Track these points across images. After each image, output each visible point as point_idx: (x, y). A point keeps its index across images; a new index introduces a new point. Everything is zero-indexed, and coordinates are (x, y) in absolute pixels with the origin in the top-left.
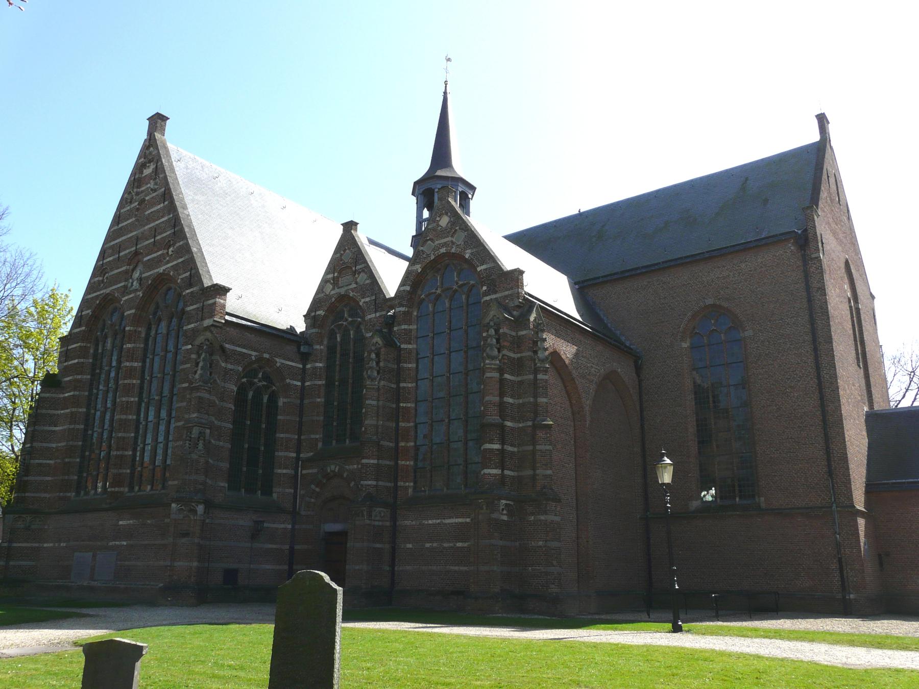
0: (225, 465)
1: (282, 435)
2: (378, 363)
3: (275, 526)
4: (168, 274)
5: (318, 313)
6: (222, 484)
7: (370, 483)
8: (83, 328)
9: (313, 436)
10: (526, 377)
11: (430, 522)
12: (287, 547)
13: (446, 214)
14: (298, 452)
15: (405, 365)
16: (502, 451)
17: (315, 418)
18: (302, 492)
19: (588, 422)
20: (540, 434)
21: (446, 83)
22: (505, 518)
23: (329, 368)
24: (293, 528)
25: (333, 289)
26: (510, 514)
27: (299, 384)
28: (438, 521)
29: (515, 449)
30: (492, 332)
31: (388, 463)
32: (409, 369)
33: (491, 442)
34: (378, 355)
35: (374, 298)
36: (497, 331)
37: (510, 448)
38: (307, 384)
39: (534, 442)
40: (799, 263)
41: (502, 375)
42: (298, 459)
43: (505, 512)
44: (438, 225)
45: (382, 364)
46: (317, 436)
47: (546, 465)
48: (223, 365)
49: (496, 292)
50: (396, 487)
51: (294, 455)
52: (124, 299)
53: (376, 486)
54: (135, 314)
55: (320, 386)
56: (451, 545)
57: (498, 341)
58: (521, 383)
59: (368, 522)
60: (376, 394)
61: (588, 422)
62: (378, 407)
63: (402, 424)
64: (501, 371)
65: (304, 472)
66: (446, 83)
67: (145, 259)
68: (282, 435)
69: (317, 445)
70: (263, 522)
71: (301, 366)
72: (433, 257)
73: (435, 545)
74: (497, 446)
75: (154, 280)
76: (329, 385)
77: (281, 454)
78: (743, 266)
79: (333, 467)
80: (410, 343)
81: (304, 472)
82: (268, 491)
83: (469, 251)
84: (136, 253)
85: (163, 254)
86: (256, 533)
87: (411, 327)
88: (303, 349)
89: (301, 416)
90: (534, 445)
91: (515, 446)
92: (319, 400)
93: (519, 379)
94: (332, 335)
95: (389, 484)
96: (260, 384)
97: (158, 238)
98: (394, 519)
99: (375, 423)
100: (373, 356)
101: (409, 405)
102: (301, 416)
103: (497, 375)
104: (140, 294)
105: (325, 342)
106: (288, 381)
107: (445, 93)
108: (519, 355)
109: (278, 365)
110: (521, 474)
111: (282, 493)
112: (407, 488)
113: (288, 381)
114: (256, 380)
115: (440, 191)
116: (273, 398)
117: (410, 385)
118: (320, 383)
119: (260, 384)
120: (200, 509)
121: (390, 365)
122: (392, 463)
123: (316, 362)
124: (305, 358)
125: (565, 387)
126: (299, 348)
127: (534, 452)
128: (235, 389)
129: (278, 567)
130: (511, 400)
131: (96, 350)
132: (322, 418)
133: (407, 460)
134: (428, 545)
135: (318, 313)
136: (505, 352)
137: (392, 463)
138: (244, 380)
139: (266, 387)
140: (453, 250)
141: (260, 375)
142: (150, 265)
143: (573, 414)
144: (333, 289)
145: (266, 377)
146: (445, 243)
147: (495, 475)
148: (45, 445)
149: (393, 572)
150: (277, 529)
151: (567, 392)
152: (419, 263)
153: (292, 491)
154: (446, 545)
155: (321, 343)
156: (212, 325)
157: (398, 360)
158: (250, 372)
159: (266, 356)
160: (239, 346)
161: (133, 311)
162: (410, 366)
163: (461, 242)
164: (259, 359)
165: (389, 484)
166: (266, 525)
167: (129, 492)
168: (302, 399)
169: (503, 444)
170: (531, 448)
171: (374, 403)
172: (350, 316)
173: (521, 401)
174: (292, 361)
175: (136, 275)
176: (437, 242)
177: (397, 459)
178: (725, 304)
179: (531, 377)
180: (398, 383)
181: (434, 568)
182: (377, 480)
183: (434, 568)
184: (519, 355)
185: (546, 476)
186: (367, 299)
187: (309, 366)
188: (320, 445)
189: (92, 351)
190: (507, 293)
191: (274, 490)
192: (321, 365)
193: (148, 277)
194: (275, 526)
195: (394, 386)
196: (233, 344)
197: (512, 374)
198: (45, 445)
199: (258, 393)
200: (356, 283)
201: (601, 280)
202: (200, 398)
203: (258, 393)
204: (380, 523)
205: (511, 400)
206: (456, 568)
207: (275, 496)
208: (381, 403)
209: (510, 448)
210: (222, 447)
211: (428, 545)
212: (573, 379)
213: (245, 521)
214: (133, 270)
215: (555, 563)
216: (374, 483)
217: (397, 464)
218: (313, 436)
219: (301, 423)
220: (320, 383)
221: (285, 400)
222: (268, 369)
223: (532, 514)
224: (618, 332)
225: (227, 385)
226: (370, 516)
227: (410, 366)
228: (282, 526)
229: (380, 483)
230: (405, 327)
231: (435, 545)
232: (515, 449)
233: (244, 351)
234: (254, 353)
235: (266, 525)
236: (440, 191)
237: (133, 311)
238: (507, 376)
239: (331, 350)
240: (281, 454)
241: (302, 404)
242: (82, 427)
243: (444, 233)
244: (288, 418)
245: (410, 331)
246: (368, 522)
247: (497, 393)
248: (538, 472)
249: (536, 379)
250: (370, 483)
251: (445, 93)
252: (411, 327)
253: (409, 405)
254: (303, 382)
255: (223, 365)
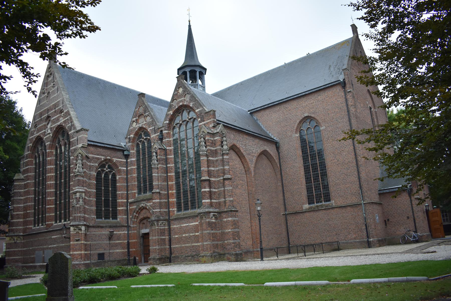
0: (94, 208)
1: (119, 192)
2: (157, 157)
3: (120, 232)
4: (62, 125)
5: (131, 136)
6: (93, 217)
7: (157, 210)
8: (29, 152)
9: (133, 192)
10: (218, 158)
11: (184, 225)
12: (126, 241)
13: (181, 87)
14: (127, 199)
15: (169, 157)
16: (210, 192)
17: (133, 183)
18: (131, 217)
19: (253, 174)
20: (227, 182)
21: (189, 22)
22: (214, 221)
23: (138, 160)
24: (128, 233)
25: (136, 125)
26: (216, 218)
27: (125, 169)
28: (188, 224)
29: (217, 190)
30: (202, 139)
31: (165, 201)
32: (171, 158)
33: (205, 188)
34: (156, 153)
35: (153, 127)
36: (204, 139)
37: (214, 190)
38: (129, 168)
39: (224, 186)
40: (343, 94)
41: (208, 158)
42: (127, 202)
43: (213, 218)
44: (178, 92)
45: (158, 157)
46: (135, 191)
47: (230, 196)
48: (89, 164)
49: (204, 121)
50: (169, 211)
51: (126, 201)
52: (45, 138)
53: (160, 211)
54: (50, 144)
55: (134, 169)
56: (194, 234)
57: (205, 143)
58: (217, 160)
59: (157, 227)
60: (157, 171)
61: (253, 174)
62: (158, 176)
63: (169, 183)
64: (207, 156)
65: (131, 208)
66: (189, 22)
67: (52, 119)
68: (119, 192)
69: (135, 195)
70: (113, 231)
71: (125, 161)
72: (177, 107)
73: (187, 235)
74: (208, 190)
75: (56, 128)
76: (138, 168)
77: (120, 201)
78: (319, 97)
79: (142, 205)
80: (170, 147)
81: (131, 208)
82: (115, 217)
83: (192, 103)
84: (49, 117)
85: (59, 116)
86: (111, 237)
87: (170, 139)
88: (126, 153)
89: (127, 183)
90: (224, 187)
91: (216, 189)
92: (134, 175)
93: (216, 159)
94: (138, 145)
95: (166, 210)
96: (107, 170)
97: (56, 109)
98: (169, 225)
99: (157, 183)
100: (154, 154)
101: (172, 174)
102: (127, 183)
103: (205, 158)
104: (51, 135)
105: (135, 149)
106: (120, 168)
107: (190, 26)
108: (215, 148)
109: (114, 161)
110: (220, 201)
111: (121, 218)
112: (174, 211)
113: (120, 168)
114: (105, 169)
115: (191, 72)
116: (114, 176)
117: (172, 165)
118: (134, 167)
119: (107, 170)
120: (83, 228)
121: (162, 157)
122: (166, 201)
123: (132, 158)
124: (127, 157)
125: (241, 160)
126: (124, 153)
127: (224, 190)
128: (96, 174)
129: (123, 250)
130: (213, 169)
131: (56, 152)
132: (136, 183)
133: (173, 199)
134: (184, 235)
135: (131, 136)
136: (208, 148)
137: (166, 201)
138: (100, 169)
139: (110, 172)
140: (185, 104)
141: (107, 167)
142: (54, 122)
143: (245, 171)
144: (136, 125)
145: (110, 167)
146: (182, 100)
147: (208, 202)
148: (19, 205)
149: (170, 248)
150: (121, 234)
151: (242, 162)
152: (171, 110)
153: (126, 217)
154: (191, 234)
155: (133, 149)
156: (82, 147)
157: (166, 154)
158: (102, 165)
159: (109, 158)
160: (95, 155)
161: (49, 143)
162: (171, 157)
163: (188, 100)
164: (105, 160)
165: (166, 210)
166: (115, 233)
167: (55, 223)
168: (127, 175)
169: (210, 188)
170: (223, 189)
171: (157, 175)
172: (145, 136)
173: (217, 169)
174: (121, 159)
175: (49, 126)
176: (178, 100)
177: (168, 198)
178: (313, 116)
179: (221, 157)
180: (167, 164)
181: (187, 245)
182: (160, 209)
183: (187, 245)
184: (215, 148)
185: (230, 201)
186: (151, 128)
187: (129, 160)
188: (137, 195)
189: (34, 162)
190: (208, 121)
191: (118, 217)
192: (134, 159)
193: (54, 127)
194: (120, 232)
195: (165, 166)
196: (93, 154)
197: (213, 157)
198: (19, 205)
199: (107, 174)
200: (146, 121)
201: (259, 109)
202: (78, 180)
203: (107, 174)
204: (163, 228)
205: (213, 169)
206: (196, 244)
207: (118, 219)
208: (159, 174)
209: (214, 190)
210: (92, 200)
211: (184, 235)
212: (244, 156)
213: (106, 232)
214: (48, 124)
215: (237, 238)
216: (159, 210)
217: (169, 201)
218: (133, 192)
219: (127, 186)
220: (134, 167)
221: (119, 177)
222: (110, 164)
223: (225, 218)
224: (268, 132)
225: (91, 173)
226: (158, 225)
227: (171, 157)
228: (123, 232)
229: (162, 210)
230: (168, 139)
231: (187, 235)
232: (217, 190)
233: (98, 157)
234: (103, 157)
235: (115, 233)
236: (191, 72)
237: (49, 143)
238: (210, 158)
239: (138, 152)
240: (120, 201)
241: (127, 177)
242: (33, 196)
243: (181, 96)
244: (121, 184)
245: (170, 141)
246: (157, 227)
247: (206, 166)
248: (226, 199)
249: (223, 158)
250: (157, 210)
251: (190, 26)
252: (170, 139)
253: (172, 174)
254: (127, 167)
255: (89, 164)
